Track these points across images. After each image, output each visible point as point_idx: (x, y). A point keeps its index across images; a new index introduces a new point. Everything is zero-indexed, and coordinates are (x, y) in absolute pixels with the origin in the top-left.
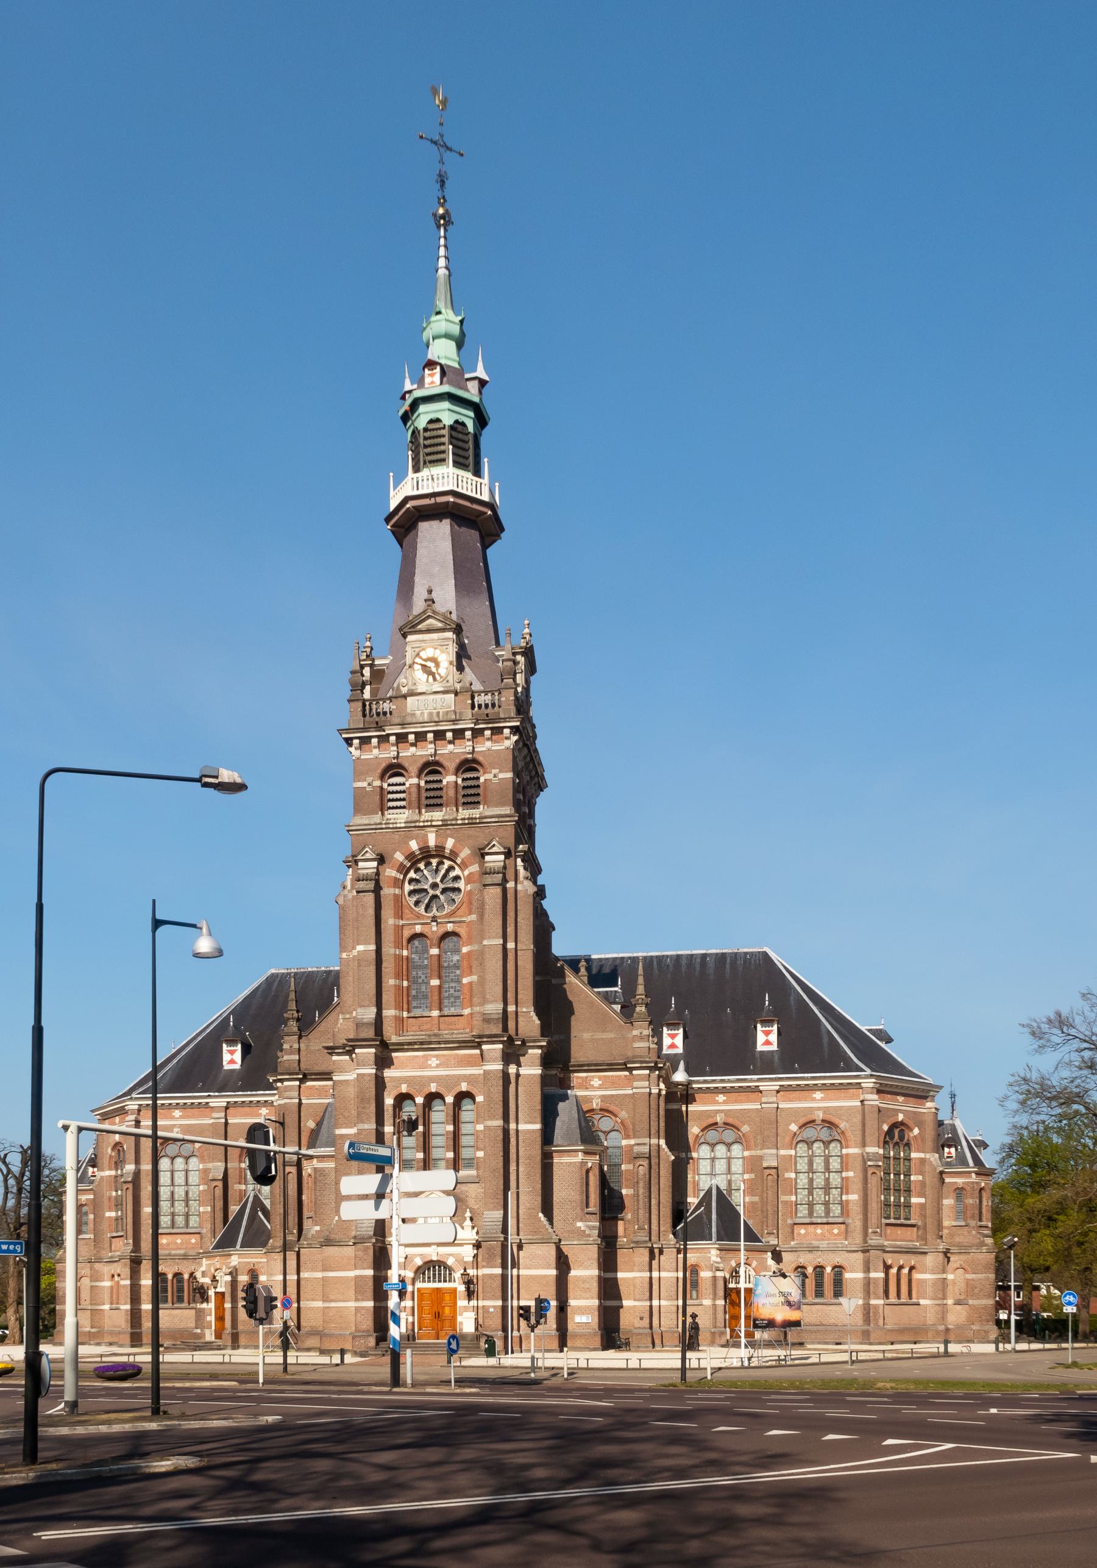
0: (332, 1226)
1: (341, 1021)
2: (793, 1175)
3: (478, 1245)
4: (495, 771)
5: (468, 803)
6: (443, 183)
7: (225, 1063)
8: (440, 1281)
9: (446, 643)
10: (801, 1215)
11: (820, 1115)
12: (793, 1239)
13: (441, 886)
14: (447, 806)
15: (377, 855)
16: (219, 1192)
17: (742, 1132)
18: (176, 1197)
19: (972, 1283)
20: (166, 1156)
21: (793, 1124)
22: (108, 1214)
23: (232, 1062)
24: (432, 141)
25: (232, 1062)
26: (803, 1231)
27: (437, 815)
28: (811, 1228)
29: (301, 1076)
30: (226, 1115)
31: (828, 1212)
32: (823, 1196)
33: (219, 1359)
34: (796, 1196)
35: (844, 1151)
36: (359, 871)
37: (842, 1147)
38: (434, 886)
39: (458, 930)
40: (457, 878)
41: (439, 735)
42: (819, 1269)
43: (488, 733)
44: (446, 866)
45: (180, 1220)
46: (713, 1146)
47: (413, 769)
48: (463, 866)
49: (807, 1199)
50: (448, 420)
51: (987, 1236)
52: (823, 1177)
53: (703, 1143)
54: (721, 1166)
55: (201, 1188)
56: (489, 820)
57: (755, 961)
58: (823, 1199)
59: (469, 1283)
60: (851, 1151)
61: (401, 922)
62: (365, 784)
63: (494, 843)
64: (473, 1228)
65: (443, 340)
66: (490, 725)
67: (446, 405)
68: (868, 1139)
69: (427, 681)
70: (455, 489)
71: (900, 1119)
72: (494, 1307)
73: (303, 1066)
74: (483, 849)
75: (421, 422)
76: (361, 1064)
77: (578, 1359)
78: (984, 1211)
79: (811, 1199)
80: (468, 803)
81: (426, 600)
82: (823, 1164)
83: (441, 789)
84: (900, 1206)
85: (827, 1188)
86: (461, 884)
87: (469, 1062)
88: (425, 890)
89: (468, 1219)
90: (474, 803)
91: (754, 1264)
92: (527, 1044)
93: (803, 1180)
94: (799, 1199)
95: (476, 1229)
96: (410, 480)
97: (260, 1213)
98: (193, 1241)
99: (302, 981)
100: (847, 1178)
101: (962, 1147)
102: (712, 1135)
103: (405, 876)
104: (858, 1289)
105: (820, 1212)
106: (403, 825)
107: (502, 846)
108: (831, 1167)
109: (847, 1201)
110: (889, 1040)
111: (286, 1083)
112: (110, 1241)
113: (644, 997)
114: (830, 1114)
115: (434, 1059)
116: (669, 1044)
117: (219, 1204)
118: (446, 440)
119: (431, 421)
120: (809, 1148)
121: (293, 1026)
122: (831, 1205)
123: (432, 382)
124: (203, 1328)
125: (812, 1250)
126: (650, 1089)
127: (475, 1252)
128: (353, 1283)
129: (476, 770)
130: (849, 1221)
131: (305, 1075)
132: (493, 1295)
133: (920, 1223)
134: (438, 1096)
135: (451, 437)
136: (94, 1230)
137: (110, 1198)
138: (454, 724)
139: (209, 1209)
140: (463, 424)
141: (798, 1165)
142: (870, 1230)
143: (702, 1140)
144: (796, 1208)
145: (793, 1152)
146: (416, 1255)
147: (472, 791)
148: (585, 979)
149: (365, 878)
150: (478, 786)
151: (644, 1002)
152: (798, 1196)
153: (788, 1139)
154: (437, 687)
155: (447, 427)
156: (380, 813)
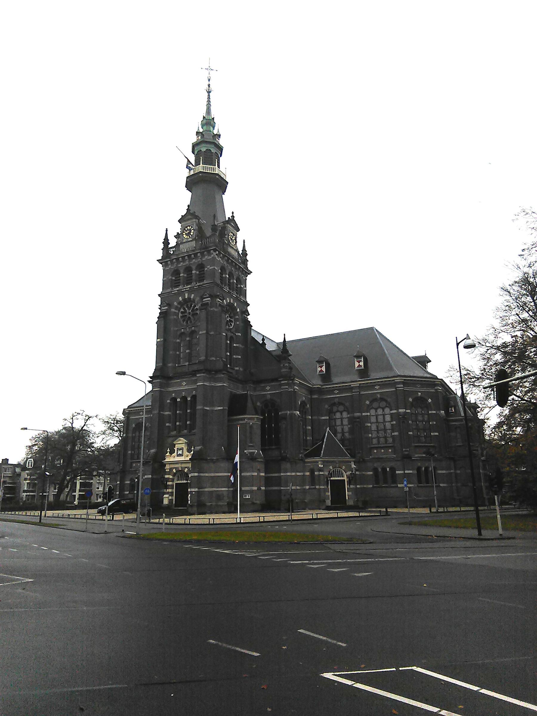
12: (371, 455)
42: (384, 469)
46: (376, 409)
47: (182, 271)
50: (204, 149)
54: (380, 419)
55: (349, 426)
58: (384, 435)
85: (385, 430)
91: (344, 467)
102: (375, 405)
103: (179, 311)
154: (190, 239)
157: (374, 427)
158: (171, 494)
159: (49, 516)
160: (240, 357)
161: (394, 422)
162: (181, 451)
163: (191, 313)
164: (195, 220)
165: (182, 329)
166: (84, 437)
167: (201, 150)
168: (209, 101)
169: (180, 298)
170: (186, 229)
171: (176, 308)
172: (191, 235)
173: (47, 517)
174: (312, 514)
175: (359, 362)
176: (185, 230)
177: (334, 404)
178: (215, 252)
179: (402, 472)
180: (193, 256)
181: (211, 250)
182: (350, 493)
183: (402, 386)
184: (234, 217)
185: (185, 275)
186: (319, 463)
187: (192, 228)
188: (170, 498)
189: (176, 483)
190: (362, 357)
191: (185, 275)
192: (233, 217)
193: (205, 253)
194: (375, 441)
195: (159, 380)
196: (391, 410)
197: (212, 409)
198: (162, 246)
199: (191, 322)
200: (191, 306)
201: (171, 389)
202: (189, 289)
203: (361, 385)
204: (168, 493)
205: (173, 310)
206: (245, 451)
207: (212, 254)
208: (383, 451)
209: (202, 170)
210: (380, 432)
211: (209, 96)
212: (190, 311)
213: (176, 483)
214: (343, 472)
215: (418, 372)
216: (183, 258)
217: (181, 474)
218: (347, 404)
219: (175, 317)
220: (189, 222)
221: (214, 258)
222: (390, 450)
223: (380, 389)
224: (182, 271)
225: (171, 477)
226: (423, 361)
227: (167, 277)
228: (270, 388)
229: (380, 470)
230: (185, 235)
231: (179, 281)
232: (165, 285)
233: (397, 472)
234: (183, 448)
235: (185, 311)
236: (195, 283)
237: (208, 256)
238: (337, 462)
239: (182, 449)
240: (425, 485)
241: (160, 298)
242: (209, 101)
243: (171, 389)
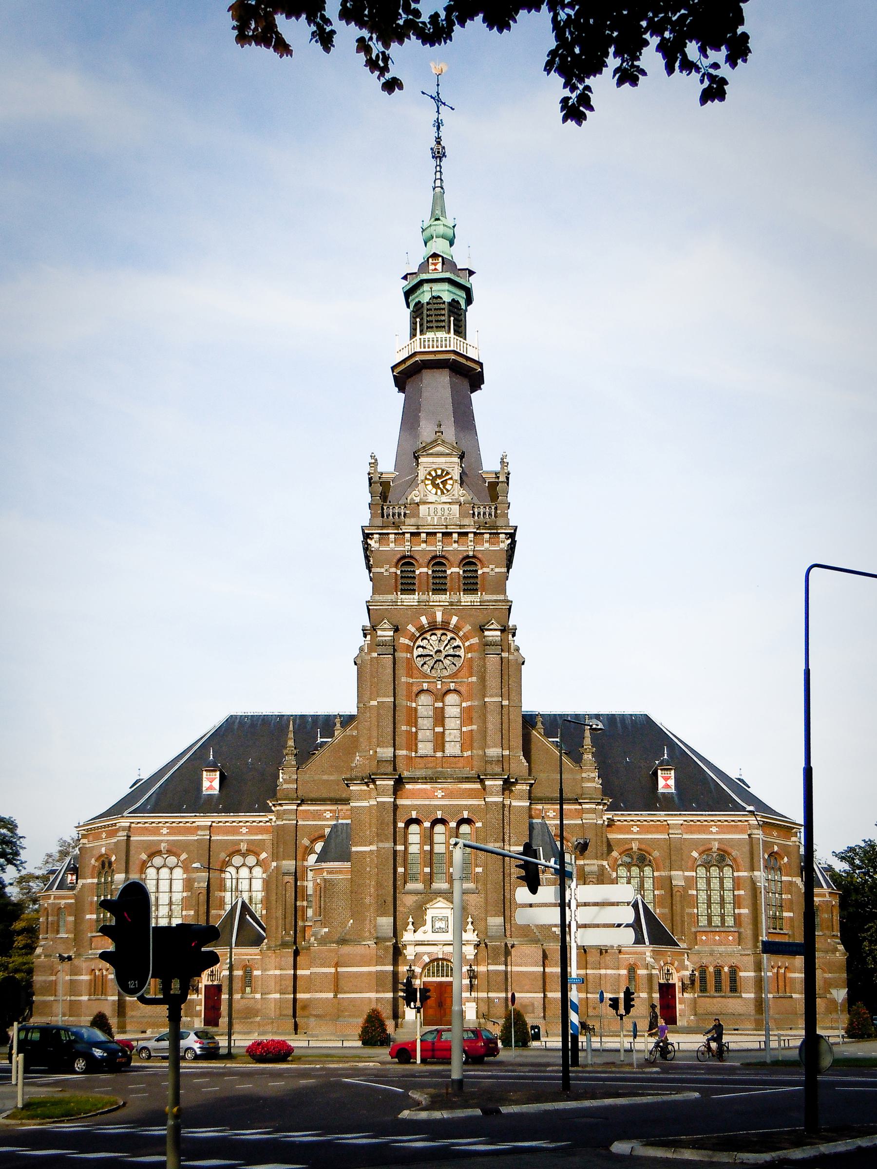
0: (348, 928)
1: (358, 758)
2: (694, 892)
3: (477, 946)
7: (204, 789)
8: (443, 976)
9: (452, 466)
10: (702, 925)
12: (696, 944)
13: (444, 653)
14: (451, 590)
15: (394, 626)
16: (203, 898)
17: (652, 856)
18: (160, 902)
19: (829, 980)
20: (152, 866)
22: (88, 917)
23: (211, 788)
24: (432, 97)
25: (211, 788)
27: (444, 598)
28: (711, 936)
30: (210, 833)
31: (723, 921)
32: (719, 909)
33: (305, 1044)
34: (698, 909)
35: (736, 874)
36: (379, 638)
37: (733, 871)
38: (439, 651)
39: (459, 688)
43: (455, 536)
45: (716, 920)
49: (706, 912)
50: (447, 298)
51: (839, 944)
52: (719, 894)
53: (150, 866)
55: (185, 894)
56: (488, 604)
57: (640, 722)
58: (719, 912)
59: (472, 975)
60: (741, 874)
61: (411, 680)
62: (382, 570)
63: (493, 621)
64: (474, 931)
65: (441, 239)
66: (489, 531)
67: (446, 286)
69: (436, 494)
70: (455, 349)
71: (775, 850)
72: (499, 998)
73: (300, 793)
74: (484, 626)
75: (425, 298)
76: (380, 792)
78: (834, 923)
79: (710, 912)
80: (467, 589)
82: (718, 884)
83: (445, 577)
84: (776, 918)
86: (461, 653)
87: (471, 794)
88: (431, 656)
89: (470, 923)
90: (473, 589)
91: (676, 963)
92: (519, 782)
93: (703, 896)
94: (699, 912)
95: (476, 932)
96: (418, 341)
97: (248, 917)
99: (259, 723)
100: (739, 896)
101: (816, 873)
104: (750, 984)
105: (717, 922)
106: (479, 604)
107: (392, 624)
108: (725, 886)
109: (739, 914)
110: (749, 787)
111: (285, 807)
112: (91, 940)
113: (590, 747)
114: (725, 844)
115: (439, 790)
116: (208, 786)
117: (203, 909)
118: (446, 312)
121: (291, 760)
122: (726, 917)
123: (436, 269)
126: (297, 821)
127: (476, 951)
128: (375, 976)
129: (475, 564)
130: (742, 930)
131: (302, 801)
132: (498, 988)
133: (790, 933)
134: (417, 821)
135: (450, 311)
136: (75, 929)
137: (92, 902)
138: (460, 528)
139: (192, 913)
140: (458, 302)
141: (698, 884)
143: (620, 862)
144: (698, 918)
145: (694, 874)
146: (425, 954)
148: (542, 731)
149: (384, 644)
150: (414, 578)
151: (591, 751)
152: (699, 909)
153: (690, 863)
154: (444, 499)
155: (446, 303)
156: (395, 593)
165: (452, 682)
166: (851, 883)
167: (419, 302)
169: (424, 620)
182: (683, 1006)
187: (428, 477)
189: (206, 986)
203: (133, 825)
205: (404, 641)
209: (421, 348)
213: (206, 986)
220: (442, 459)
239: (446, 919)
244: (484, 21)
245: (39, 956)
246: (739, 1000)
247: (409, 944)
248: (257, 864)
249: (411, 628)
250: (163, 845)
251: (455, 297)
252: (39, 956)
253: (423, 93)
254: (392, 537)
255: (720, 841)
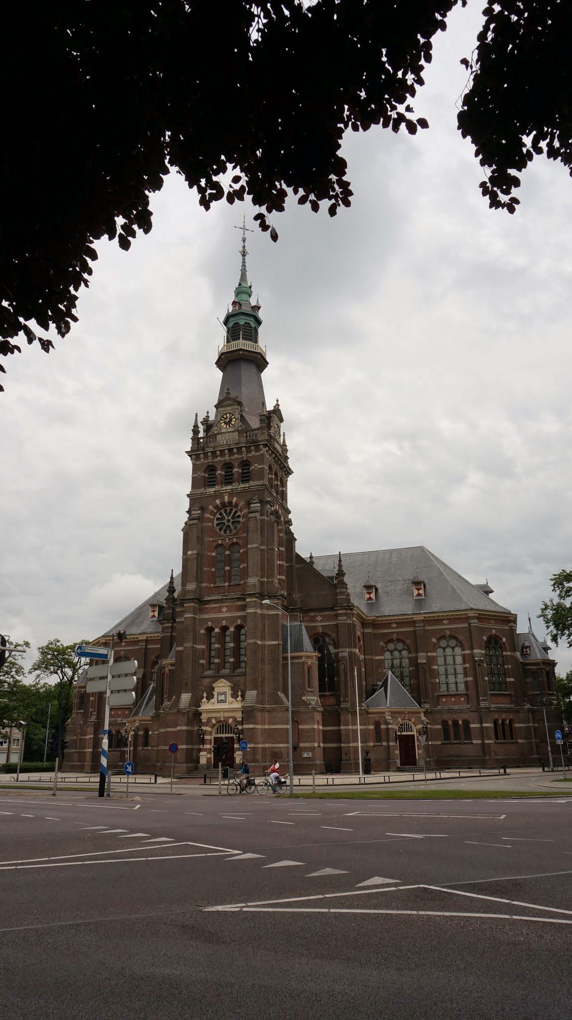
4: (256, 465)
5: (244, 481)
6: (244, 241)
11: (395, 636)
21: (434, 639)
26: (444, 700)
27: (211, 490)
28: (449, 698)
29: (172, 621)
40: (239, 516)
41: (230, 450)
42: (455, 723)
44: (233, 511)
45: (452, 687)
48: (241, 510)
50: (242, 322)
53: (386, 651)
68: (474, 646)
70: (243, 348)
77: (327, 779)
80: (244, 481)
81: (226, 393)
86: (241, 519)
90: (213, 485)
91: (413, 720)
98: (127, 712)
102: (443, 643)
103: (215, 517)
119: (235, 324)
120: (392, 654)
124: (124, 762)
125: (450, 711)
140: (249, 324)
142: (481, 698)
146: (213, 718)
147: (246, 475)
154: (230, 430)
157: (442, 670)
158: (209, 751)
159: (21, 780)
160: (284, 578)
161: (467, 665)
162: (224, 696)
163: (231, 520)
164: (237, 407)
165: (235, 538)
168: (244, 265)
169: (218, 502)
170: (225, 416)
171: (212, 513)
172: (232, 424)
173: (20, 781)
174: (327, 779)
175: (418, 589)
176: (223, 417)
177: (391, 641)
178: (265, 447)
179: (478, 725)
180: (235, 450)
181: (260, 445)
182: (421, 751)
183: (422, 625)
184: (279, 405)
185: (223, 473)
186: (387, 714)
187: (233, 417)
188: (209, 756)
190: (157, 607)
191: (207, 475)
192: (278, 405)
193: (253, 448)
194: (443, 688)
195: (192, 604)
196: (463, 650)
197: (264, 643)
198: (191, 435)
199: (231, 531)
200: (230, 512)
201: (206, 616)
202: (230, 490)
204: (205, 750)
206: (304, 698)
207: (262, 450)
208: (453, 700)
210: (449, 677)
211: (244, 259)
212: (230, 518)
214: (413, 725)
215: (480, 604)
216: (222, 451)
217: (223, 726)
218: (408, 641)
219: (210, 524)
220: (229, 408)
221: (263, 455)
222: (462, 699)
223: (448, 624)
224: (219, 467)
225: (209, 729)
226: (487, 591)
227: (199, 473)
228: (321, 618)
229: (450, 723)
230: (223, 424)
231: (231, 477)
232: (195, 483)
233: (472, 726)
234: (226, 692)
235: (223, 518)
236: (238, 484)
237: (256, 452)
238: (406, 712)
239: (225, 693)
240: (503, 741)
241: (188, 499)
242: (244, 265)
243: (206, 616)
244: (562, 161)
245: (68, 725)
246: (471, 746)
247: (204, 712)
248: (404, 649)
249: (211, 507)
250: (122, 652)
251: (246, 321)
252: (68, 725)
253: (235, 227)
254: (202, 455)
255: (450, 629)
